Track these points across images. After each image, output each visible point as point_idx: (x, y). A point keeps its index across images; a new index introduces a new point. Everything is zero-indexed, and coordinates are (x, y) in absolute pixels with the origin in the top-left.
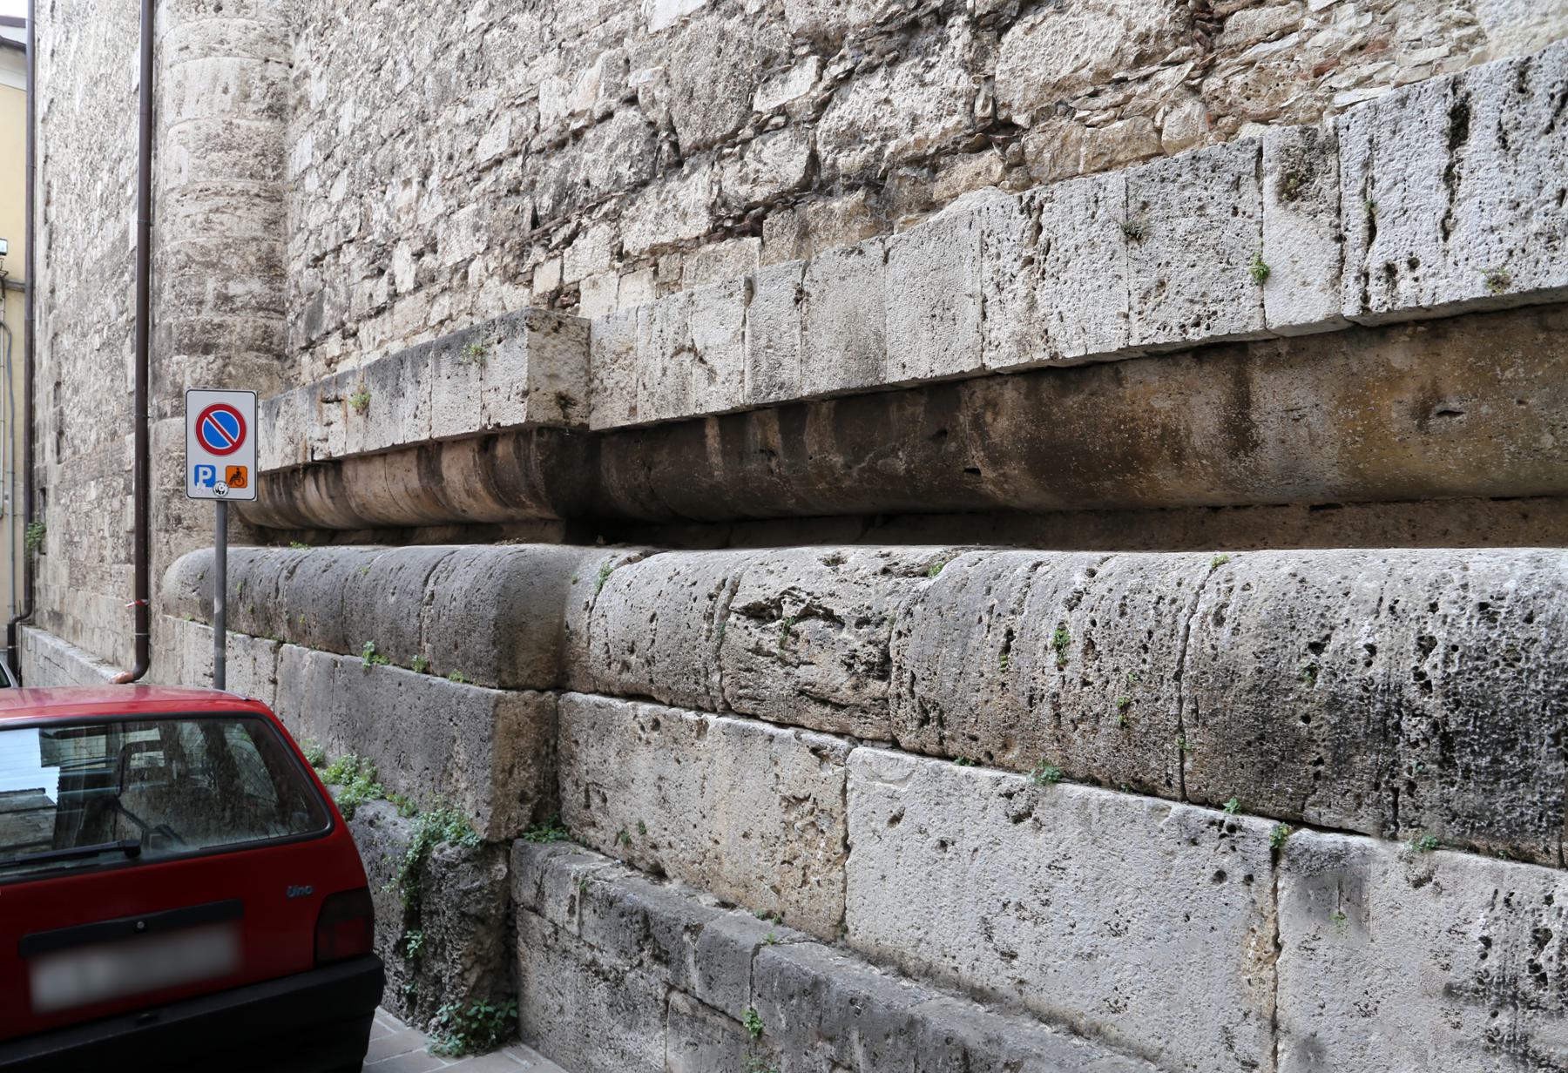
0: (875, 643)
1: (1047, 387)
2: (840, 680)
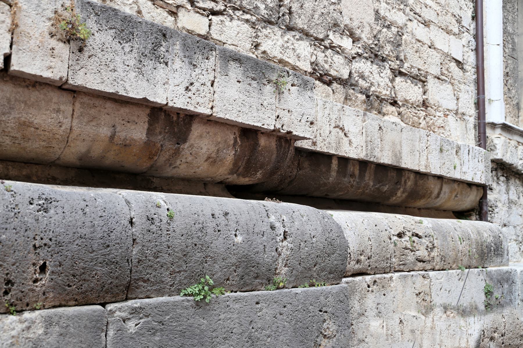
0: (430, 242)
1: (418, 176)
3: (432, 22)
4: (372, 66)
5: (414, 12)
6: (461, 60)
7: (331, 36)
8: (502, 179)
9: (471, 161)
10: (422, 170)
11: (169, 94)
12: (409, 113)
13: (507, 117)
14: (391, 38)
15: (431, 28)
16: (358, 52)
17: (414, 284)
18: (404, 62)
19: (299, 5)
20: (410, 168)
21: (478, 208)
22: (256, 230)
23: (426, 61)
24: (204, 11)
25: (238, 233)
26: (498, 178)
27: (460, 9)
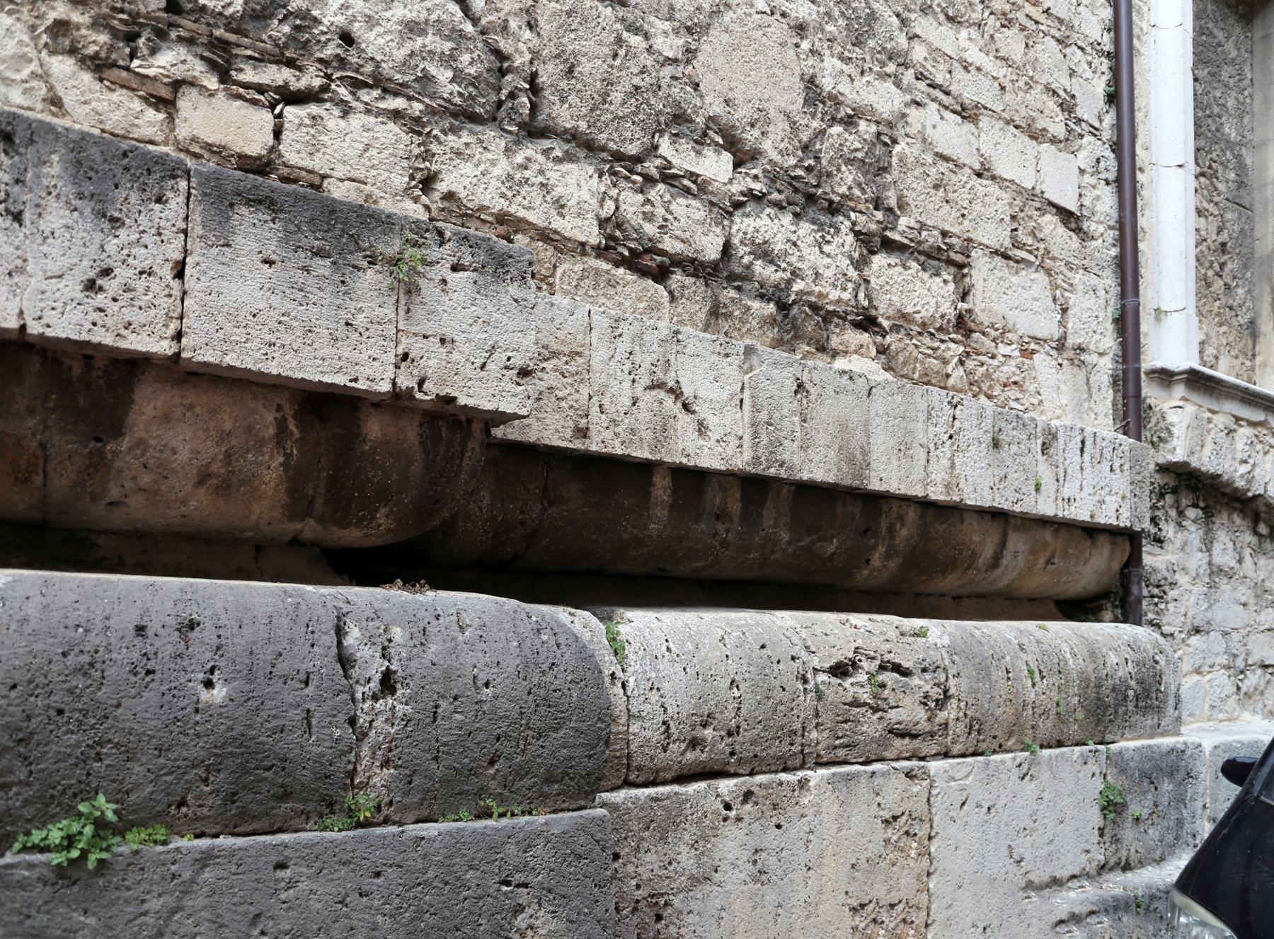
0: (938, 685)
2: (920, 716)
3: (986, 108)
4: (797, 225)
5: (928, 82)
6: (1072, 206)
7: (665, 147)
8: (1192, 513)
9: (1088, 471)
10: (933, 497)
11: (29, 300)
12: (911, 348)
13: (1222, 357)
14: (857, 150)
15: (981, 124)
16: (752, 190)
17: (878, 794)
18: (899, 213)
19: (561, 67)
20: (897, 492)
21: (1121, 591)
22: (282, 668)
23: (965, 212)
24: (261, 92)
25: (215, 678)
26: (1181, 513)
27: (1071, 76)
